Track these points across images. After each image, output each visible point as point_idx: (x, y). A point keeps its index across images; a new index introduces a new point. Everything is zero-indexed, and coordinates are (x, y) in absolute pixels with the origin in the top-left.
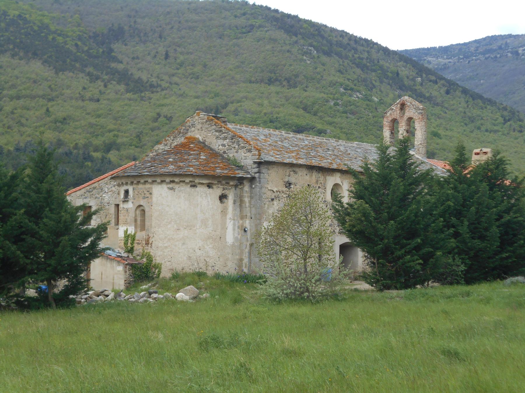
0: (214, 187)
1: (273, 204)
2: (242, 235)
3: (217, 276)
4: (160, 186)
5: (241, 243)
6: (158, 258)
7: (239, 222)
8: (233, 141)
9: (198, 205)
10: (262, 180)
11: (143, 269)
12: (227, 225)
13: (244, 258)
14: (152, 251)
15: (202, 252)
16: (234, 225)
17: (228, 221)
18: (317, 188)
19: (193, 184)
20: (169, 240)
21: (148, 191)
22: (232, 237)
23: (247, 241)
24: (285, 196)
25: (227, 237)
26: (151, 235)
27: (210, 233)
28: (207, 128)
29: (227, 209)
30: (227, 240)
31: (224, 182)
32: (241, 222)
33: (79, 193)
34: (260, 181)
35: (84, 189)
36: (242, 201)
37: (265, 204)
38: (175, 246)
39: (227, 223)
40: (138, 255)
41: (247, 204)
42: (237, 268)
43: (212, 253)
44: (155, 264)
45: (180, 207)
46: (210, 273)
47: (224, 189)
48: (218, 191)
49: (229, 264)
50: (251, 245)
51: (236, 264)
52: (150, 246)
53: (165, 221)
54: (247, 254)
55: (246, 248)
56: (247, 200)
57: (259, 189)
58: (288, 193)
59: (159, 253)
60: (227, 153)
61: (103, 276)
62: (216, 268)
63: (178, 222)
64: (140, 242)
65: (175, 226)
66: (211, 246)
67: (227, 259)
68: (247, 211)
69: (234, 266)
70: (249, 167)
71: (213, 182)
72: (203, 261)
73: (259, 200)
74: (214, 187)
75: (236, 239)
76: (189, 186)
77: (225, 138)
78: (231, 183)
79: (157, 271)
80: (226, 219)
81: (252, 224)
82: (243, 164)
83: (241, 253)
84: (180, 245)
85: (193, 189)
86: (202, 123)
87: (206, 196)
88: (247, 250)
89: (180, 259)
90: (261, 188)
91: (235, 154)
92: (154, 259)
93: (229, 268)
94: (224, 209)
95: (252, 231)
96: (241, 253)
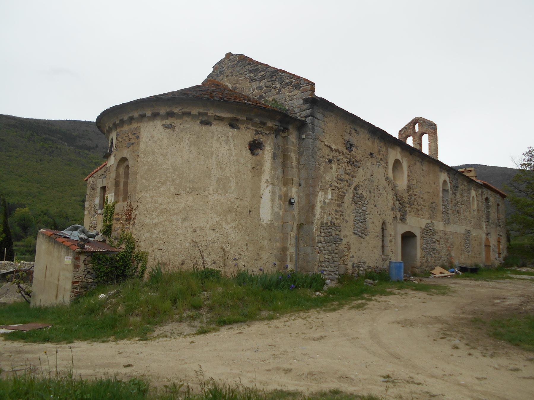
0: (241, 126)
1: (331, 168)
2: (286, 211)
3: (242, 278)
4: (151, 123)
5: (284, 223)
6: (142, 244)
7: (280, 189)
8: (273, 79)
9: (212, 153)
10: (316, 128)
11: (117, 261)
12: (262, 192)
13: (288, 246)
14: (134, 231)
15: (218, 235)
16: (273, 192)
17: (263, 185)
18: (379, 159)
19: (205, 118)
20: (161, 212)
21: (134, 134)
22: (270, 212)
23: (294, 220)
24: (345, 159)
25: (262, 211)
26: (134, 205)
27: (232, 203)
28: (238, 71)
29: (262, 166)
30: (262, 216)
31: (257, 120)
32: (284, 189)
33: (100, 173)
34: (313, 129)
35: (104, 168)
36: (285, 157)
37: (319, 165)
38: (172, 222)
39: (262, 189)
40: (116, 239)
41: (294, 163)
42: (277, 263)
43: (235, 236)
44: (138, 254)
45: (182, 157)
46: (230, 271)
47: (257, 133)
48: (246, 135)
49: (265, 255)
50: (300, 226)
51: (276, 256)
52: (132, 222)
53: (157, 180)
54: (293, 241)
55: (292, 231)
56: (293, 156)
57: (311, 140)
58: (349, 156)
59: (145, 235)
60: (264, 98)
61: (48, 272)
62: (241, 263)
63: (177, 181)
64: (120, 216)
65: (172, 189)
66: (233, 225)
67: (262, 248)
68: (293, 173)
69: (273, 260)
70: (297, 110)
71: (238, 117)
72: (219, 250)
73: (313, 157)
74: (241, 126)
75: (275, 215)
76: (198, 122)
77: (263, 78)
78: (270, 124)
79: (140, 265)
80: (260, 181)
81: (301, 194)
82: (287, 107)
83: (285, 238)
84: (180, 221)
85: (205, 128)
86: (233, 67)
87: (227, 141)
88: (293, 234)
89: (179, 246)
90: (315, 139)
91: (276, 97)
92: (136, 245)
93: (261, 261)
94: (257, 165)
95: (301, 205)
96: (285, 238)
